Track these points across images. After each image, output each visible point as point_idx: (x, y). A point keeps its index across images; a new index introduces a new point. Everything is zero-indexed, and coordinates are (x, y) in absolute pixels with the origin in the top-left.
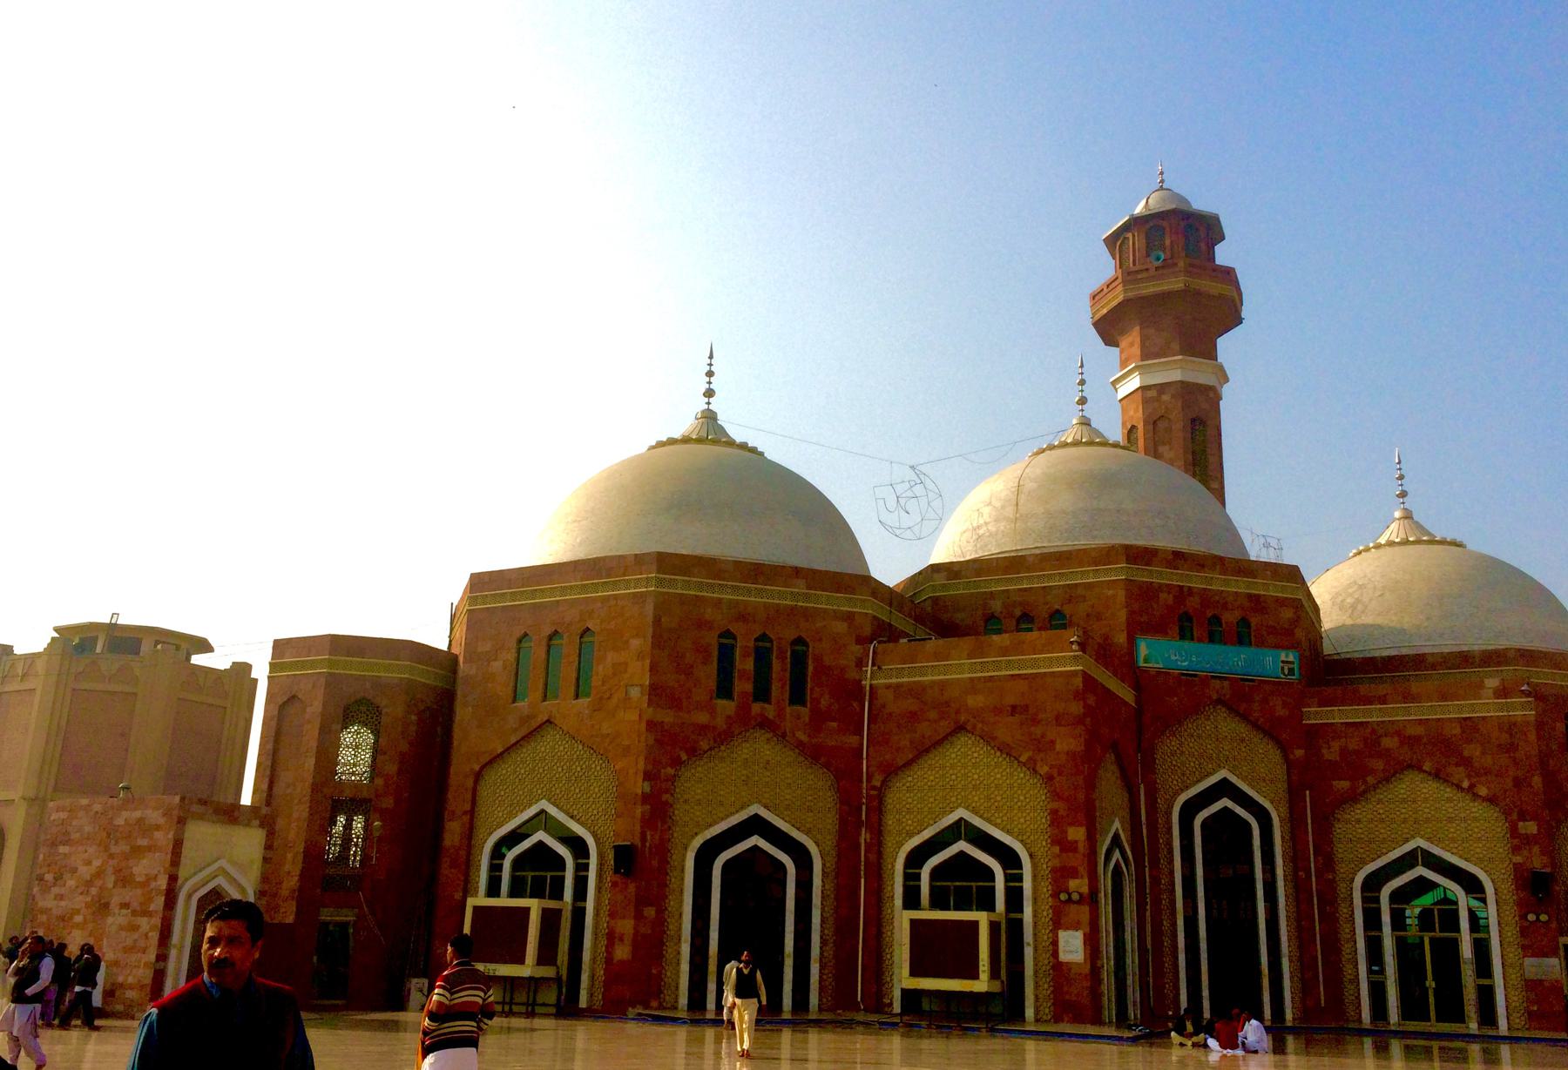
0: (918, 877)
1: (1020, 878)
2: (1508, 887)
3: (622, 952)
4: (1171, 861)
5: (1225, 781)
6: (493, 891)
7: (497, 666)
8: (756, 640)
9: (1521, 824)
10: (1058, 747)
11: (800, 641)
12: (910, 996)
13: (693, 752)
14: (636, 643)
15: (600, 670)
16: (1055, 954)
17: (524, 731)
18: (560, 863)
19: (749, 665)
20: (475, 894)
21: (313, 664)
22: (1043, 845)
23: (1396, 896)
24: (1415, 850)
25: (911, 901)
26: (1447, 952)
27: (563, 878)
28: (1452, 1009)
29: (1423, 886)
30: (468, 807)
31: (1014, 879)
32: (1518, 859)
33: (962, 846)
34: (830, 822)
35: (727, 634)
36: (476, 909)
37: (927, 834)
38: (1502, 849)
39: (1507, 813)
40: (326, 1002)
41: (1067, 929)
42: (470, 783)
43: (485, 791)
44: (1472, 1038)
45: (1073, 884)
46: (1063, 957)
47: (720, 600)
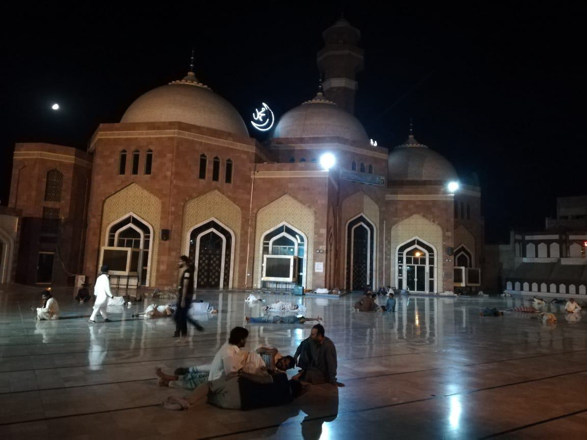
0: (114, 236)
1: (433, 255)
2: (441, 251)
3: (163, 267)
4: (345, 241)
5: (361, 217)
6: (111, 243)
7: (112, 161)
8: (215, 158)
9: (447, 233)
10: (319, 202)
11: (229, 160)
12: (264, 284)
13: (191, 198)
14: (169, 155)
15: (154, 165)
16: (314, 269)
17: (123, 186)
18: (138, 235)
19: (212, 167)
20: (104, 245)
21: (21, 155)
22: (311, 234)
23: (408, 254)
24: (415, 240)
25: (266, 250)
26: (421, 270)
27: (139, 241)
28: (421, 287)
29: (416, 250)
30: (100, 214)
31: (432, 256)
32: (444, 243)
33: (131, 225)
34: (239, 224)
35: (203, 155)
36: (105, 251)
37: (272, 230)
38: (440, 240)
39: (443, 229)
40: (368, 272)
41: (318, 261)
42: (101, 205)
43: (106, 208)
44: (427, 295)
45: (321, 247)
46: (316, 271)
47: (201, 142)
